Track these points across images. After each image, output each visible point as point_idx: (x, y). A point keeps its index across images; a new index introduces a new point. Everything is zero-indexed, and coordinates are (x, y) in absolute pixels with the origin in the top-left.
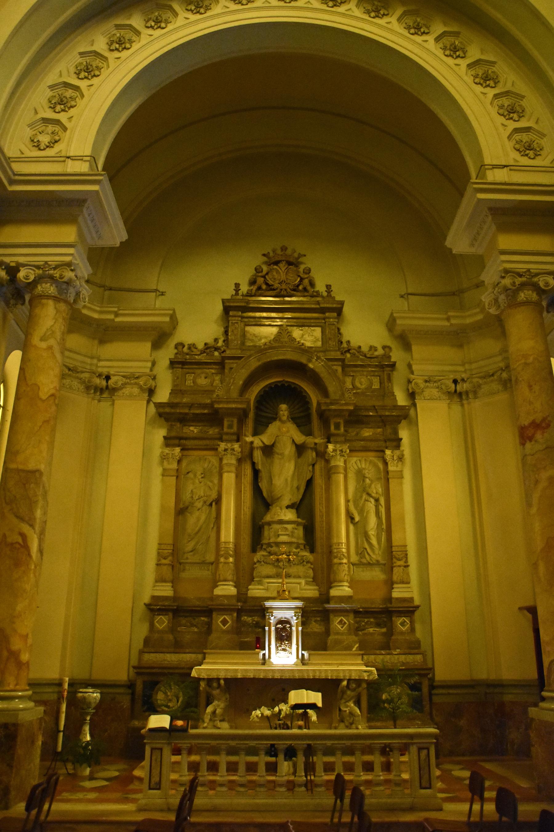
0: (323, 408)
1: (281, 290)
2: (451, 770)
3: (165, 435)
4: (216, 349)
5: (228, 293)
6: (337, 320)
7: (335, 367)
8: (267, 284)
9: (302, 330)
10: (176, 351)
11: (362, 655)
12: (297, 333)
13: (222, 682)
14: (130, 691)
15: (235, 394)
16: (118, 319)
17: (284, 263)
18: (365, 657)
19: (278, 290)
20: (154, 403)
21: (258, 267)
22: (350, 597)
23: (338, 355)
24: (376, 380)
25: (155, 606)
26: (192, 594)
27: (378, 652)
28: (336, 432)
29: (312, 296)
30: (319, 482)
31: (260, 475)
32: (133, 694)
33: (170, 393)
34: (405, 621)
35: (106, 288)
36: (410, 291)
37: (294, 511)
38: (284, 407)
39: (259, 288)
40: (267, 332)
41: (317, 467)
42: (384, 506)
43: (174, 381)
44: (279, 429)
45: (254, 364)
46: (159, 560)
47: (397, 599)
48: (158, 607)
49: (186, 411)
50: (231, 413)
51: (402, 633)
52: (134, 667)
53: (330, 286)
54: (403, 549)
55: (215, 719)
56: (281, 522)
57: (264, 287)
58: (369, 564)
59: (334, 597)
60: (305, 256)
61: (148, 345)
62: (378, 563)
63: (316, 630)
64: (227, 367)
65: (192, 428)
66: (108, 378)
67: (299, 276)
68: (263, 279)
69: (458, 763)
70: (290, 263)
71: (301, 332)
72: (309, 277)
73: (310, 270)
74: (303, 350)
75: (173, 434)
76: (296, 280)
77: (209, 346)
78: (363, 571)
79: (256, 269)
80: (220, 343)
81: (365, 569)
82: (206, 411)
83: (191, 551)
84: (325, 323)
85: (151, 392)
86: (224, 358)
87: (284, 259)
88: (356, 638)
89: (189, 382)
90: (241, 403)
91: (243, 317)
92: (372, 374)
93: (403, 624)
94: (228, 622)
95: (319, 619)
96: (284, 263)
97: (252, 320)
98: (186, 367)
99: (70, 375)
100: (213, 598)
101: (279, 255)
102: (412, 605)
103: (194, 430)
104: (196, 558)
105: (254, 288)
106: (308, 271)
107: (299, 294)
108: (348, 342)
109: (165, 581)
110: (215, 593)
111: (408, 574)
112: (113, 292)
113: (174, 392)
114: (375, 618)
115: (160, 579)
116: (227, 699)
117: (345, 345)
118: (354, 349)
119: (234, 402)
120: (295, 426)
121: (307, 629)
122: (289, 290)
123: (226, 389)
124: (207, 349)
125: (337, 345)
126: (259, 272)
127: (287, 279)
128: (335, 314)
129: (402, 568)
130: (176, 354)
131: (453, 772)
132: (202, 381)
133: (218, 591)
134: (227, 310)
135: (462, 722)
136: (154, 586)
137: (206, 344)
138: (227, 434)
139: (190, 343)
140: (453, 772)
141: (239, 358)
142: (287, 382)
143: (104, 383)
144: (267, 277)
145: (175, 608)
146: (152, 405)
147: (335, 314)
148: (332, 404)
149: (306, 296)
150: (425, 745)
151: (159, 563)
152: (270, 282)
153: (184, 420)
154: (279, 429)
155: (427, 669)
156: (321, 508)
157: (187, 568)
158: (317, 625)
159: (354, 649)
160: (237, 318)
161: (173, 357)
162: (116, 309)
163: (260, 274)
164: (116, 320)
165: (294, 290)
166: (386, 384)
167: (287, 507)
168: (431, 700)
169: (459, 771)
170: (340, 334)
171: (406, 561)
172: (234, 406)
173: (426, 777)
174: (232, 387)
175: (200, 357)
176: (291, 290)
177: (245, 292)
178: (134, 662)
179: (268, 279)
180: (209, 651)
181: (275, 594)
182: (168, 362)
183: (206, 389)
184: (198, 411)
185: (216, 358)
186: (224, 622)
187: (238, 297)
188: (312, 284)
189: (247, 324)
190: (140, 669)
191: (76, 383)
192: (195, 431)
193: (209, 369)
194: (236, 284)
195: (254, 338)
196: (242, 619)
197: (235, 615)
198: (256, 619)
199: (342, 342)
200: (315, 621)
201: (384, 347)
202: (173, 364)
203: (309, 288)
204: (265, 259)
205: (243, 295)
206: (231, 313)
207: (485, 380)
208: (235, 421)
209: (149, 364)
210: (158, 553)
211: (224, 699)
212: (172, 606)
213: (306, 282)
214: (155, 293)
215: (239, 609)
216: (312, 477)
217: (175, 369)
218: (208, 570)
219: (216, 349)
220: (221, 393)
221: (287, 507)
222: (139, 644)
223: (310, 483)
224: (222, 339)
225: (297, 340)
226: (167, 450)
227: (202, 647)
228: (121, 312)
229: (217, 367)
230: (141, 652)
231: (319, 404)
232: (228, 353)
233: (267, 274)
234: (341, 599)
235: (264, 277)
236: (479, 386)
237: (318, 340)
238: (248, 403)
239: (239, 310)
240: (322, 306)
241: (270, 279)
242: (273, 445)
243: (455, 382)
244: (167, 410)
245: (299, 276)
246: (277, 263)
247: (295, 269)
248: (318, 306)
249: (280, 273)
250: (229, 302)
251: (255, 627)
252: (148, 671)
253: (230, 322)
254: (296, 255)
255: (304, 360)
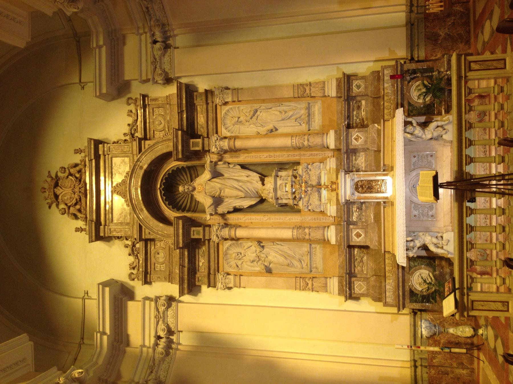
0: (180, 156)
1: (80, 192)
2: (484, 41)
3: (206, 286)
4: (134, 245)
5: (84, 237)
6: (106, 145)
7: (147, 147)
8: (76, 204)
9: (115, 174)
10: (136, 280)
11: (384, 121)
12: (118, 179)
13: (409, 239)
14: (419, 313)
15: (170, 230)
16: (108, 331)
17: (55, 190)
18: (386, 117)
19: (81, 194)
20: (180, 297)
21: (61, 212)
22: (336, 132)
23: (135, 144)
24: (157, 111)
25: (346, 292)
26: (336, 262)
27: (382, 108)
28: (201, 145)
29: (85, 165)
30: (243, 158)
31: (238, 207)
32: (421, 310)
33: (172, 283)
34: (356, 85)
35: (82, 342)
36: (78, 81)
37: (266, 179)
38: (181, 189)
39: (79, 211)
40: (119, 203)
41: (230, 160)
42: (260, 105)
43: (161, 281)
44: (199, 192)
45: (145, 214)
46: (309, 289)
47: (337, 92)
48: (348, 290)
49: (186, 269)
50: (186, 233)
51: (366, 88)
52: (399, 310)
53: (75, 150)
54: (296, 88)
55: (441, 243)
56: (275, 190)
57: (78, 207)
58: (309, 115)
59: (335, 146)
60: (49, 172)
61: (130, 304)
62: (308, 108)
63: (364, 159)
64: (148, 237)
65: (201, 264)
66: (159, 338)
67: (67, 177)
68: (71, 208)
69: (476, 37)
70: (56, 185)
71: (117, 174)
72: (68, 168)
73: (62, 168)
74: (131, 174)
75: (206, 280)
76: (72, 180)
77: (131, 252)
78: (314, 121)
79: (63, 214)
80: (129, 243)
81: (313, 120)
82: (186, 253)
83: (301, 262)
84: (108, 154)
85: (170, 299)
86: (141, 239)
87: (52, 190)
88: (370, 126)
89: (162, 268)
90: (178, 224)
91: (105, 225)
92: (151, 114)
93: (358, 87)
94: (358, 232)
95: (354, 158)
96: (55, 190)
97: (107, 217)
98: (149, 271)
99: (157, 372)
100: (339, 244)
101: (49, 195)
102: (343, 79)
103: (202, 262)
104: (306, 259)
105: (79, 215)
106: (63, 169)
107: (83, 177)
108: (125, 134)
109: (326, 284)
110: (334, 243)
111: (317, 83)
112: (85, 337)
113: (170, 279)
114: (353, 111)
115: (325, 288)
116: (423, 234)
117: (128, 138)
118: (131, 130)
119: (178, 230)
120: (197, 179)
121: (362, 167)
122: (80, 186)
123: (166, 239)
124: (133, 253)
125: (127, 144)
126: (65, 211)
127: (70, 187)
128: (101, 146)
129: (311, 88)
130: (138, 279)
131: (486, 40)
132: (161, 257)
133: (333, 241)
134: (98, 238)
135: (442, 33)
136: (330, 293)
137: (130, 255)
138: (204, 236)
139: (129, 269)
140: (486, 40)
141: (141, 227)
142: (161, 186)
143: (163, 340)
144: (69, 205)
145: (347, 276)
146: (182, 298)
147: (101, 146)
148: (177, 149)
149: (85, 170)
150: (467, 65)
151: (311, 288)
152: (74, 201)
153: (193, 271)
154: (199, 192)
155: (397, 64)
156: (264, 157)
157: (314, 266)
158: (359, 159)
159: (379, 128)
160: (106, 230)
161: (141, 282)
162: (99, 335)
163: (67, 210)
164: (109, 334)
165: (80, 181)
166: (160, 102)
167: (263, 184)
168: (422, 61)
169: (485, 34)
170: (118, 142)
171: (307, 85)
172: (181, 231)
173: (495, 64)
174: (165, 232)
175: (141, 259)
176: (79, 184)
177: (84, 223)
178: (395, 310)
179: (71, 203)
180: (383, 248)
181: (334, 194)
182: (147, 286)
183: (168, 253)
184: (186, 260)
185: (142, 244)
186: (358, 235)
187: (87, 229)
188: (76, 165)
189: (111, 221)
190: (400, 306)
191: (164, 366)
192: (203, 261)
193: (150, 252)
194: (76, 231)
195: (123, 214)
196: (355, 220)
197: (351, 226)
198: (354, 209)
199: (125, 140)
200: (356, 160)
201: (129, 104)
202: (147, 282)
203: (78, 168)
204: (54, 205)
205: (86, 225)
206: (102, 234)
207: (152, 15)
208: (193, 229)
209: (147, 302)
210: (303, 290)
211: (423, 237)
212: (346, 278)
213: (72, 171)
214: (86, 300)
215: (347, 223)
216: (239, 165)
217: (152, 280)
218: (316, 248)
219: (134, 245)
220: (170, 241)
221: (263, 184)
222: (379, 306)
223: (243, 166)
224: (125, 241)
225: (124, 178)
226: (219, 285)
227: (381, 255)
228: (101, 330)
229: (149, 245)
230: (386, 304)
231: (178, 160)
232: (136, 236)
233: (66, 204)
234: (338, 139)
235: (69, 207)
236: (158, 20)
237: (123, 161)
238: (178, 218)
239: (99, 228)
240: (93, 157)
241: (71, 201)
242: (213, 197)
243: (155, 42)
244: (186, 286)
245: (67, 177)
246: (56, 197)
247: (61, 180)
248: (94, 161)
249: (66, 194)
250: (92, 237)
251: (361, 210)
252: (401, 298)
253: (109, 235)
254: (49, 180)
255: (141, 173)
